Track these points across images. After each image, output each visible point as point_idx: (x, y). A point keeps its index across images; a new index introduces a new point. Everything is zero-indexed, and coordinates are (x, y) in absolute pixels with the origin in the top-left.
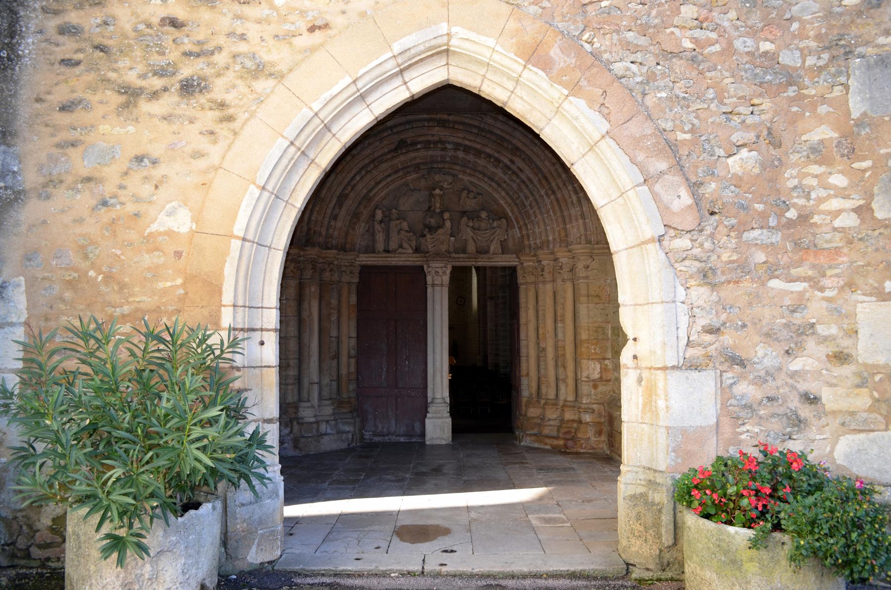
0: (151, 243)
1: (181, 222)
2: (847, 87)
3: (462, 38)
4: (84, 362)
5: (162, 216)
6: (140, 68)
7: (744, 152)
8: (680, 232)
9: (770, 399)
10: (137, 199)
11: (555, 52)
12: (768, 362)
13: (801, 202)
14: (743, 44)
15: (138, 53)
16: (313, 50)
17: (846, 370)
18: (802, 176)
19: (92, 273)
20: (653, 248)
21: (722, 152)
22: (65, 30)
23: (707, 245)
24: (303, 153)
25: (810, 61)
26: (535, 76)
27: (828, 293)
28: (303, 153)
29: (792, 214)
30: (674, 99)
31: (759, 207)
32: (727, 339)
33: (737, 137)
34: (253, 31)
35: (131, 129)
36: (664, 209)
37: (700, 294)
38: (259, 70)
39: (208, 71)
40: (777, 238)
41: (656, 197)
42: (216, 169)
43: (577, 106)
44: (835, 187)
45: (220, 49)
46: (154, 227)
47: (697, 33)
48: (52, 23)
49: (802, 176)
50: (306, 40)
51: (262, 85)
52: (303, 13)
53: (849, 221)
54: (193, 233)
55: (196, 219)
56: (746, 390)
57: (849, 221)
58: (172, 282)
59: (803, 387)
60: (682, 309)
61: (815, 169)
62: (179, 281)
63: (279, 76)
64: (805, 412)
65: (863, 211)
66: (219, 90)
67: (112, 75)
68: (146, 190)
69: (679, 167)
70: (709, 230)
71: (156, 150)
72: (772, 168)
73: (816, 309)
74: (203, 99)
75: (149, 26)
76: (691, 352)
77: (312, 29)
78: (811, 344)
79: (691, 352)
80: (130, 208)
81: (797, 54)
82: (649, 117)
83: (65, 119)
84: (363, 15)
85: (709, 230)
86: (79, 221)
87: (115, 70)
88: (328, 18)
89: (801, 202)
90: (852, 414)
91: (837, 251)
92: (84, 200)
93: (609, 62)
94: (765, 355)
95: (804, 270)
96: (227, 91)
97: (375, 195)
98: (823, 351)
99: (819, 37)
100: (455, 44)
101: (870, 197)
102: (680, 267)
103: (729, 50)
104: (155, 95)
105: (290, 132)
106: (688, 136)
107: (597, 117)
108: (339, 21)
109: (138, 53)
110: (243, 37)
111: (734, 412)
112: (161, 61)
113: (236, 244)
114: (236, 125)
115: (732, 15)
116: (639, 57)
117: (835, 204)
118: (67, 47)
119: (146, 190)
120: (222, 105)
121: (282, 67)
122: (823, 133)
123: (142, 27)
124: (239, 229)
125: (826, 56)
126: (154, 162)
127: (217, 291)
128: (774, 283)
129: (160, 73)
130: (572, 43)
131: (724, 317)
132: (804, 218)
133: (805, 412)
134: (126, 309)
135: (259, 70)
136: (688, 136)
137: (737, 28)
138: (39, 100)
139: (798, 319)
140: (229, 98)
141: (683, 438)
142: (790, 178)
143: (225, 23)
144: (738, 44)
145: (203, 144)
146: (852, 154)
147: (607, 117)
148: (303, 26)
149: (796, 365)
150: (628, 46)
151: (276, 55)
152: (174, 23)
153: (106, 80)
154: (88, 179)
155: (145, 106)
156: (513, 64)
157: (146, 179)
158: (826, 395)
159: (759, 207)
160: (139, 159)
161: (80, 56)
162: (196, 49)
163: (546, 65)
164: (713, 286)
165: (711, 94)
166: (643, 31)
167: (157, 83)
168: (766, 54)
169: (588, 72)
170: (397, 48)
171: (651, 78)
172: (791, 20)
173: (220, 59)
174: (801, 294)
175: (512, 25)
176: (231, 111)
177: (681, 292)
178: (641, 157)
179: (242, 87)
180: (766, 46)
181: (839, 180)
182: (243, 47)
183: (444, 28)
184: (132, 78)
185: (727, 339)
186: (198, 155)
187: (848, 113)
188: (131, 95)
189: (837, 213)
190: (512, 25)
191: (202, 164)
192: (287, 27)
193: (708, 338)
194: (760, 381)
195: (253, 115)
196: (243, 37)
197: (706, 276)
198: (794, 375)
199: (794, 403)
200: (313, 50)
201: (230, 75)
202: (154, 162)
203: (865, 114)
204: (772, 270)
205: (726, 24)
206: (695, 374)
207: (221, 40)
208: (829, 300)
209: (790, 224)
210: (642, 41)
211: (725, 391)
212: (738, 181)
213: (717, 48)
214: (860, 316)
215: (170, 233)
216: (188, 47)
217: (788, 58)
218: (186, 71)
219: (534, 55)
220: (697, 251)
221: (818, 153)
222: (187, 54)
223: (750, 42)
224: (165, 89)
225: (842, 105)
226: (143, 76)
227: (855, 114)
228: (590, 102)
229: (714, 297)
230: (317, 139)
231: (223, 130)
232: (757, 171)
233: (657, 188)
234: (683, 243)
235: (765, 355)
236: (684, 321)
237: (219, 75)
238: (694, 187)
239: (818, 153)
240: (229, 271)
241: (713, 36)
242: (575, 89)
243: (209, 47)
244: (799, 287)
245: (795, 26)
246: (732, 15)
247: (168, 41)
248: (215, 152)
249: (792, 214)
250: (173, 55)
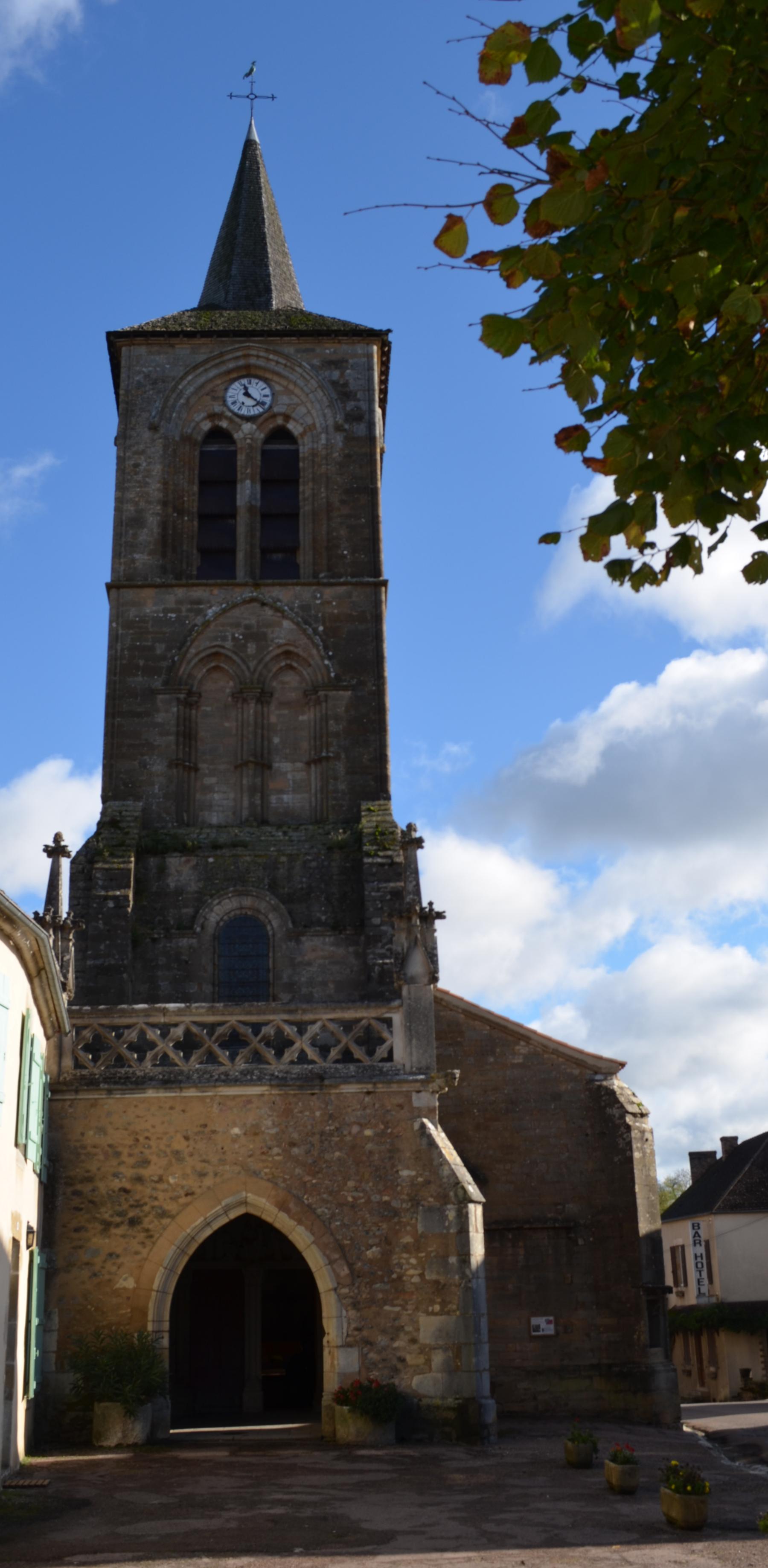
0: (117, 1293)
1: (130, 1284)
2: (417, 1219)
3: (251, 1197)
4: (572, 1557)
5: (121, 1281)
6: (110, 1212)
7: (374, 1249)
8: (344, 1286)
9: (384, 1360)
10: (110, 1273)
11: (291, 1205)
12: (383, 1343)
13: (398, 1270)
14: (375, 1198)
15: (109, 1205)
16: (187, 1204)
17: (415, 1347)
18: (400, 1258)
19: (89, 1307)
20: (332, 1293)
21: (363, 1249)
22: (77, 1193)
23: (356, 1291)
24: (183, 1251)
25: (404, 1205)
26: (283, 1216)
27: (410, 1312)
28: (183, 1251)
29: (394, 1276)
30: (344, 1225)
31: (380, 1273)
32: (365, 1333)
33: (370, 1242)
34: (161, 1196)
35: (107, 1241)
36: (337, 1276)
37: (352, 1313)
38: (164, 1214)
39: (141, 1214)
40: (387, 1287)
41: (334, 1271)
42: (145, 1259)
43: (301, 1229)
44: (412, 1264)
45: (146, 1204)
46: (118, 1286)
47: (355, 1194)
48: (69, 1190)
49: (400, 1258)
50: (183, 1200)
51: (166, 1221)
52: (183, 1187)
53: (416, 1280)
54: (135, 1289)
55: (137, 1282)
56: (373, 1356)
57: (416, 1280)
58: (125, 1311)
59: (399, 1354)
60: (344, 1320)
61: (405, 1255)
62: (129, 1310)
63: (173, 1217)
64: (400, 1366)
65: (422, 1275)
66: (146, 1223)
67: (98, 1216)
68: (114, 1269)
69: (344, 1256)
70: (357, 1285)
71: (119, 1251)
72: (386, 1255)
73: (404, 1320)
74: (139, 1227)
75: (114, 1192)
76: (349, 1339)
77: (187, 1195)
78: (402, 1335)
79: (349, 1339)
80: (107, 1277)
81: (399, 1202)
82: (332, 1234)
83: (75, 1235)
84: (209, 1188)
85: (357, 1285)
86: (83, 1283)
87: (99, 1213)
88: (194, 1189)
89: (398, 1270)
90: (418, 1366)
91: (412, 1293)
92: (85, 1273)
93: (315, 1209)
94: (382, 1340)
95: (399, 1302)
96: (150, 1224)
97: (185, 387)
98: (407, 1338)
99: (408, 1195)
100: (248, 1200)
101: (424, 1269)
102: (344, 1301)
103: (369, 1201)
104: (118, 1225)
105: (177, 1242)
106: (348, 1242)
107: (308, 1234)
108: (198, 1191)
109: (109, 1205)
110: (156, 1199)
111: (366, 1365)
112: (120, 1209)
113: (154, 1294)
114: (154, 1239)
115: (371, 1184)
116: (328, 1205)
117: (411, 1272)
118: (76, 1202)
119: (114, 1269)
120: (147, 1230)
121: (174, 1213)
122: (408, 1239)
123: (110, 1192)
124: (155, 1286)
125: (410, 1204)
126: (118, 1256)
127: (145, 1314)
128: (387, 1308)
129: (120, 1214)
130: (299, 1200)
131: (363, 1323)
132: (400, 1278)
133: (400, 1366)
134: (105, 1323)
135: (164, 1214)
136: (348, 1242)
137: (372, 1190)
138: (64, 1226)
139: (397, 1323)
140: (151, 1227)
141: (343, 1375)
142: (395, 1259)
143: (148, 1191)
144: (373, 1198)
145: (139, 1248)
146: (418, 1250)
147: (313, 1234)
148: (182, 1193)
149: (396, 1344)
150: (324, 1201)
151: (171, 1207)
152: (125, 1191)
153: (95, 1218)
154: (87, 1264)
155: (114, 1231)
156: (274, 1210)
157: (114, 1264)
158: (408, 1358)
159: (380, 1273)
160: (110, 1255)
161: (82, 1206)
162: (135, 1204)
163: (287, 1211)
164: (358, 1310)
165: (359, 1222)
166: (331, 1193)
167: (118, 1219)
168: (386, 1202)
169: (306, 1214)
170: (223, 1204)
171: (333, 1216)
172: (397, 1185)
173: (146, 1208)
174: (398, 1313)
175: (273, 1193)
176: (152, 1233)
177: (344, 1312)
178: (328, 1252)
179: (156, 1222)
180: (386, 1198)
181: (413, 1261)
182: (156, 1203)
183: (244, 1194)
184: (107, 1216)
185: (365, 1333)
186: (137, 1253)
187: (417, 1231)
188: (107, 1225)
189: (412, 1276)
190: (273, 1193)
191: (138, 1257)
192: (176, 1193)
193: (356, 1333)
194: (379, 1352)
195: (161, 1235)
196: (156, 1199)
197: (355, 1305)
198: (395, 1349)
199: (395, 1362)
200: (187, 1204)
201: (151, 1217)
202: (118, 1256)
203: (423, 1232)
204: (385, 1302)
205: (368, 1189)
206: (349, 1349)
207: (147, 1200)
208: (409, 1315)
209: (394, 1280)
210: (330, 1198)
211: (363, 1357)
212: (371, 1261)
213: (363, 1201)
214: (421, 1323)
215: (125, 1289)
216: (132, 1202)
217: (395, 1204)
218: (131, 1214)
219: (282, 1206)
220: (352, 1294)
221: (406, 1248)
222: (131, 1206)
223: (378, 1197)
224: (122, 1223)
225: (415, 1227)
226: (112, 1216)
227: (420, 1232)
228: (307, 1228)
229: (359, 1315)
230: (189, 1243)
231: (148, 1242)
232: (379, 1256)
233: (335, 1266)
234: (345, 1291)
235: (382, 1340)
236: (345, 1325)
237: (146, 1216)
238: (351, 1266)
239: (406, 1248)
240: (151, 1305)
241: (361, 1195)
242: (300, 1222)
243: (141, 1203)
244: (397, 1309)
245: (399, 1188)
246: (371, 1184)
247: (122, 1199)
248: (145, 1252)
249: (394, 1276)
250: (125, 1206)
